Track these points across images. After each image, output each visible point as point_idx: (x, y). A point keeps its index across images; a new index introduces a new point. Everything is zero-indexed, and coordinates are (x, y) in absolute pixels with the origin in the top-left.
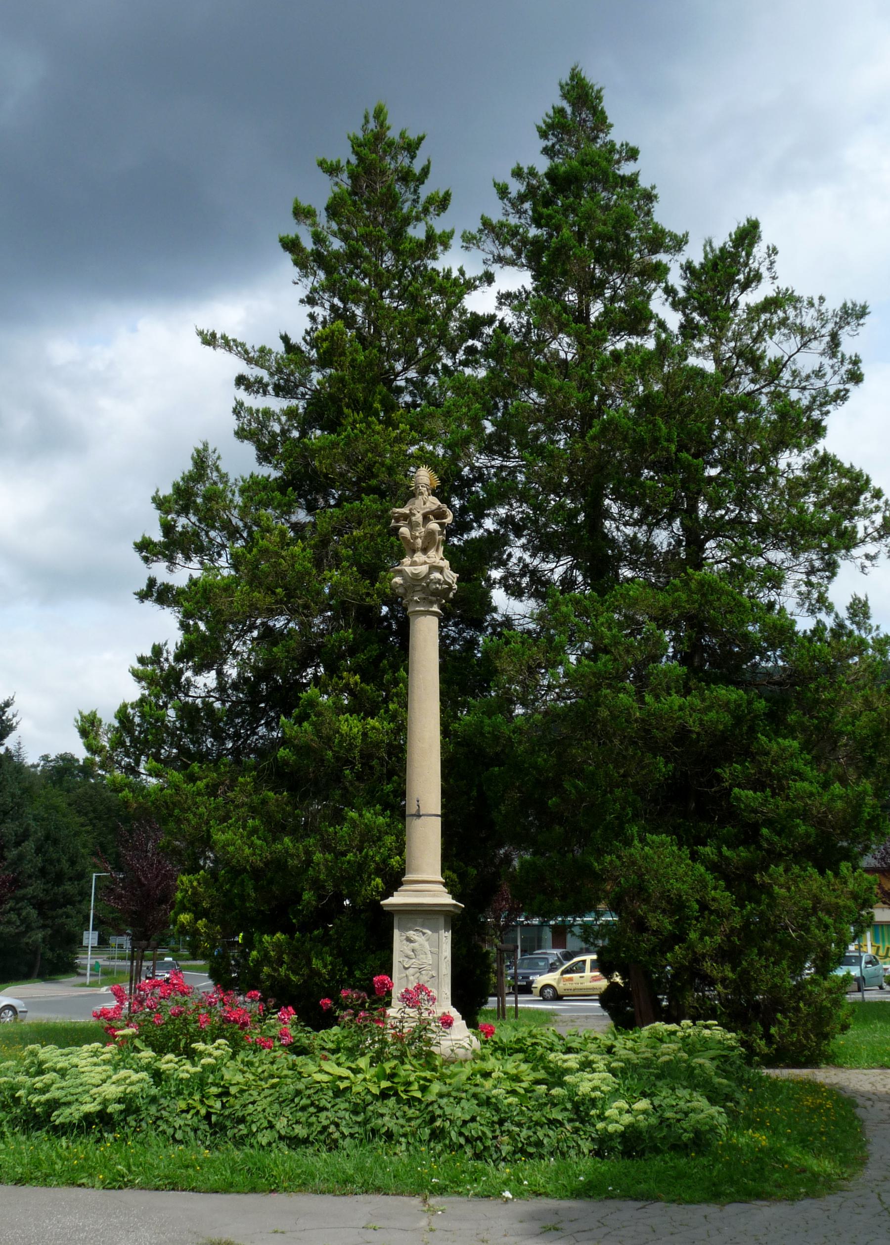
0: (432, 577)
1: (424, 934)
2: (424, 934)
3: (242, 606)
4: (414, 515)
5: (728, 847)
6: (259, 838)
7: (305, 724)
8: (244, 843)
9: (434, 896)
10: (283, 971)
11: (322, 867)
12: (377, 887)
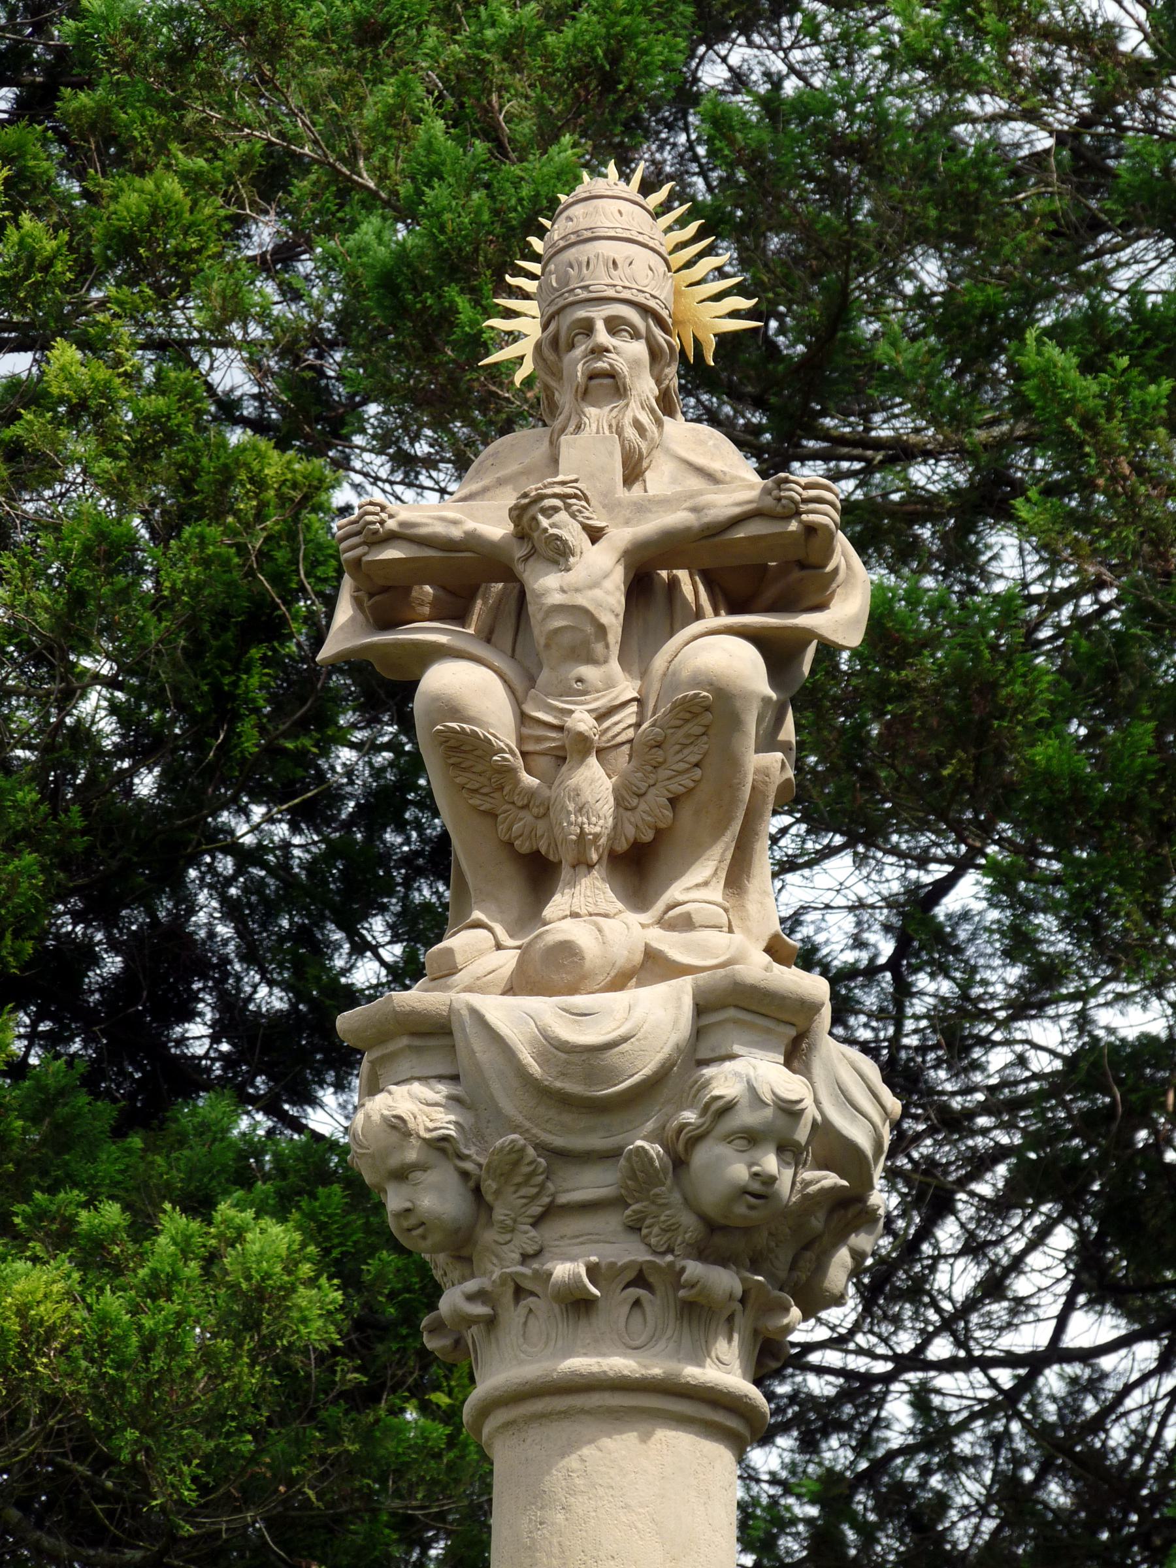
0: (724, 1081)
4: (558, 554)
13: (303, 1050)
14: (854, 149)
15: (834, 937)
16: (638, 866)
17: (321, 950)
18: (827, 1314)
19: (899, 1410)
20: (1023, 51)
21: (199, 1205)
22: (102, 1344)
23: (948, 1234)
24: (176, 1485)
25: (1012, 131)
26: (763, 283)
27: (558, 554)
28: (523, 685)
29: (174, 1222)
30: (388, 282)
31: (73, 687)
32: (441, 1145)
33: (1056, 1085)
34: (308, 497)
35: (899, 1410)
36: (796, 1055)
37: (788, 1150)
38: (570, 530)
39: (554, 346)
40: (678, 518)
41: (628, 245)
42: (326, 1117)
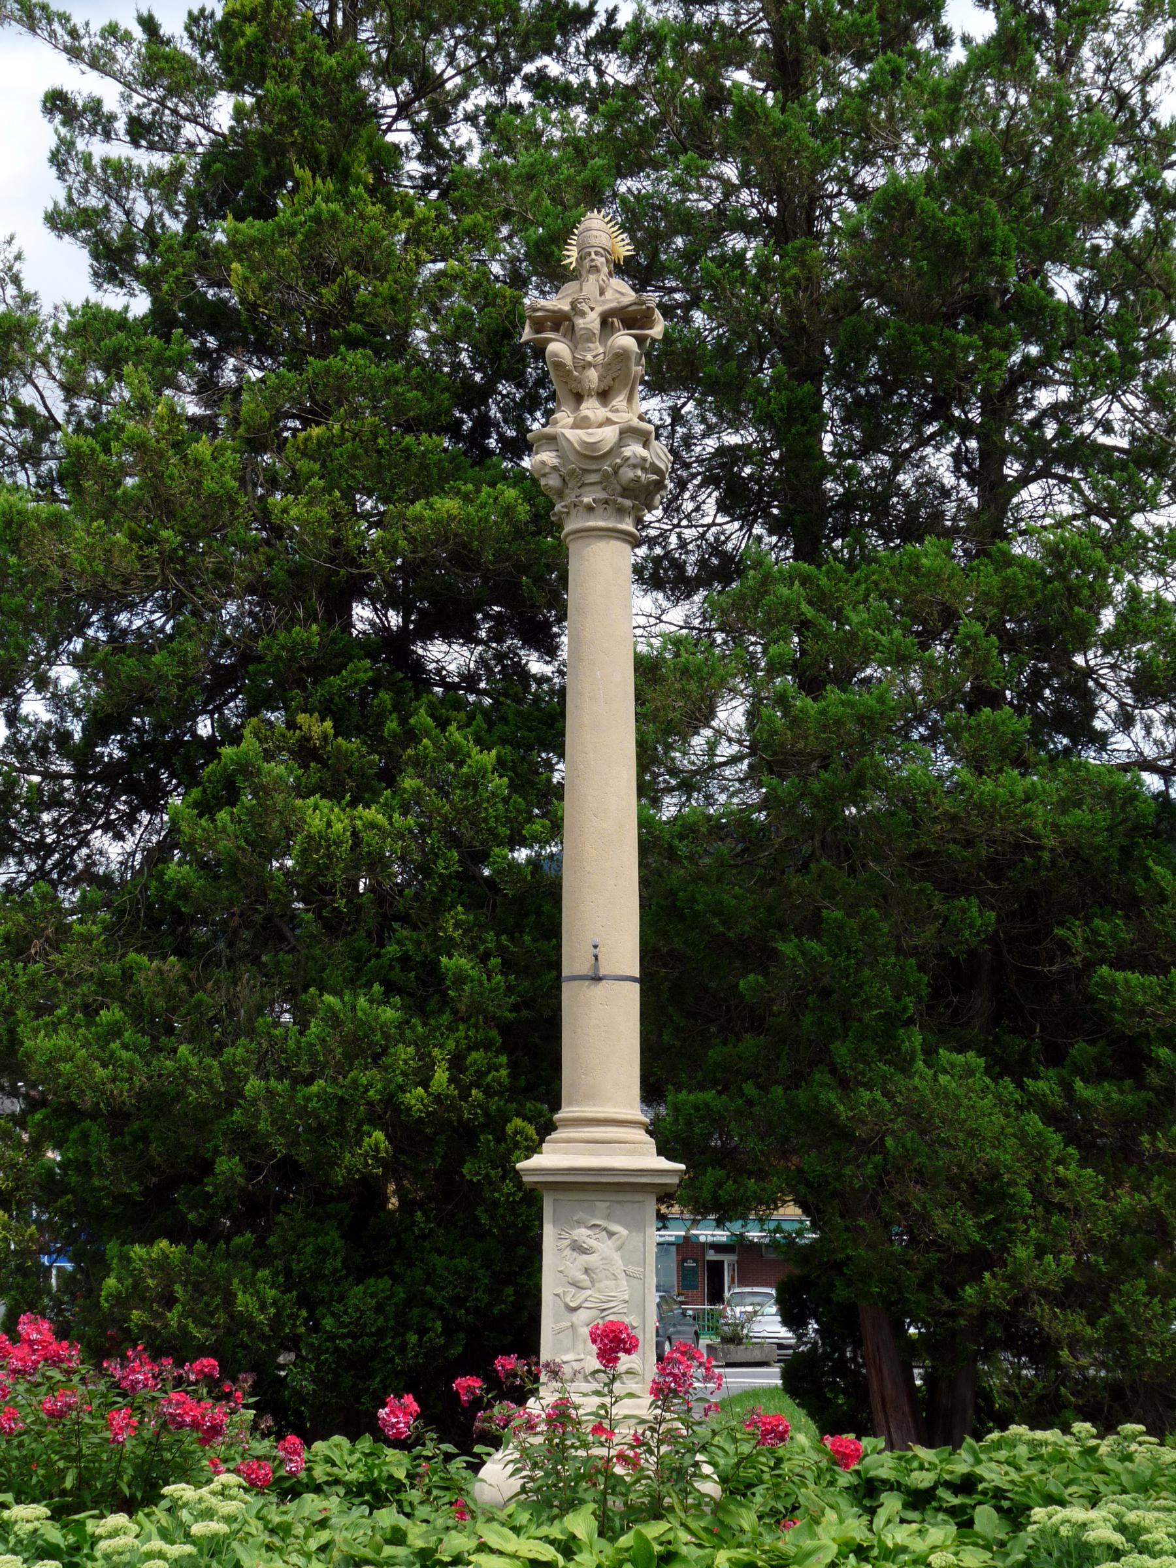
0: (627, 452)
1: (611, 1234)
2: (611, 1234)
3: (90, 560)
4: (583, 314)
5: (1086, 1081)
6: (125, 1047)
7: (223, 816)
8: (92, 1056)
9: (631, 1153)
10: (173, 1316)
11: (262, 1106)
12: (377, 1150)
13: (520, 446)
14: (659, 208)
15: (655, 418)
16: (604, 396)
17: (524, 420)
18: (855, 1480)
19: (673, 539)
20: (704, 182)
21: (493, 485)
22: (468, 521)
23: (687, 495)
24: (488, 555)
25: (702, 204)
26: (638, 245)
27: (583, 314)
28: (574, 349)
29: (486, 489)
30: (536, 244)
31: (457, 352)
32: (555, 468)
33: (713, 456)
34: (517, 301)
35: (673, 539)
36: (646, 445)
37: (643, 469)
38: (586, 309)
39: (581, 259)
40: (613, 305)
41: (601, 231)
42: (526, 463)
